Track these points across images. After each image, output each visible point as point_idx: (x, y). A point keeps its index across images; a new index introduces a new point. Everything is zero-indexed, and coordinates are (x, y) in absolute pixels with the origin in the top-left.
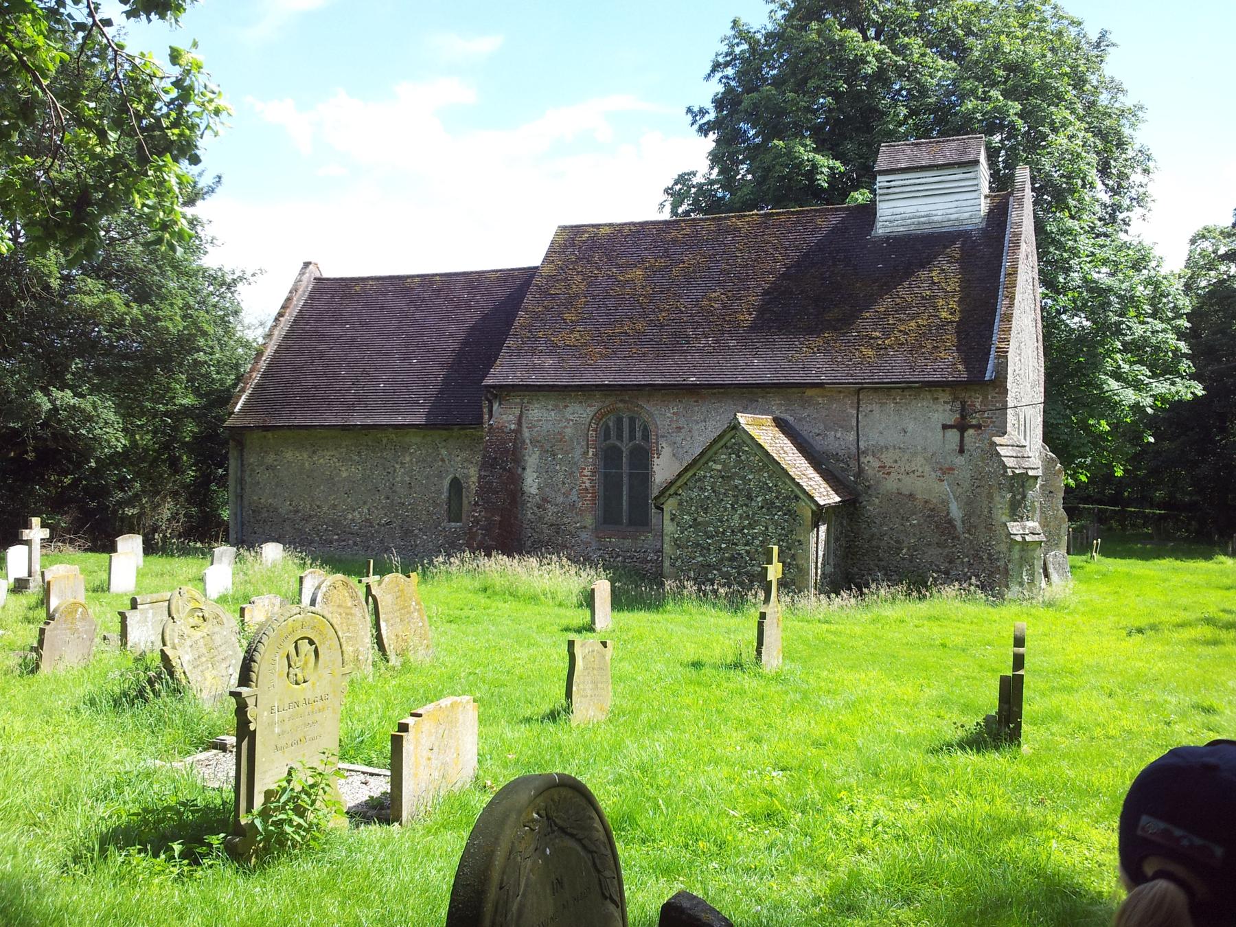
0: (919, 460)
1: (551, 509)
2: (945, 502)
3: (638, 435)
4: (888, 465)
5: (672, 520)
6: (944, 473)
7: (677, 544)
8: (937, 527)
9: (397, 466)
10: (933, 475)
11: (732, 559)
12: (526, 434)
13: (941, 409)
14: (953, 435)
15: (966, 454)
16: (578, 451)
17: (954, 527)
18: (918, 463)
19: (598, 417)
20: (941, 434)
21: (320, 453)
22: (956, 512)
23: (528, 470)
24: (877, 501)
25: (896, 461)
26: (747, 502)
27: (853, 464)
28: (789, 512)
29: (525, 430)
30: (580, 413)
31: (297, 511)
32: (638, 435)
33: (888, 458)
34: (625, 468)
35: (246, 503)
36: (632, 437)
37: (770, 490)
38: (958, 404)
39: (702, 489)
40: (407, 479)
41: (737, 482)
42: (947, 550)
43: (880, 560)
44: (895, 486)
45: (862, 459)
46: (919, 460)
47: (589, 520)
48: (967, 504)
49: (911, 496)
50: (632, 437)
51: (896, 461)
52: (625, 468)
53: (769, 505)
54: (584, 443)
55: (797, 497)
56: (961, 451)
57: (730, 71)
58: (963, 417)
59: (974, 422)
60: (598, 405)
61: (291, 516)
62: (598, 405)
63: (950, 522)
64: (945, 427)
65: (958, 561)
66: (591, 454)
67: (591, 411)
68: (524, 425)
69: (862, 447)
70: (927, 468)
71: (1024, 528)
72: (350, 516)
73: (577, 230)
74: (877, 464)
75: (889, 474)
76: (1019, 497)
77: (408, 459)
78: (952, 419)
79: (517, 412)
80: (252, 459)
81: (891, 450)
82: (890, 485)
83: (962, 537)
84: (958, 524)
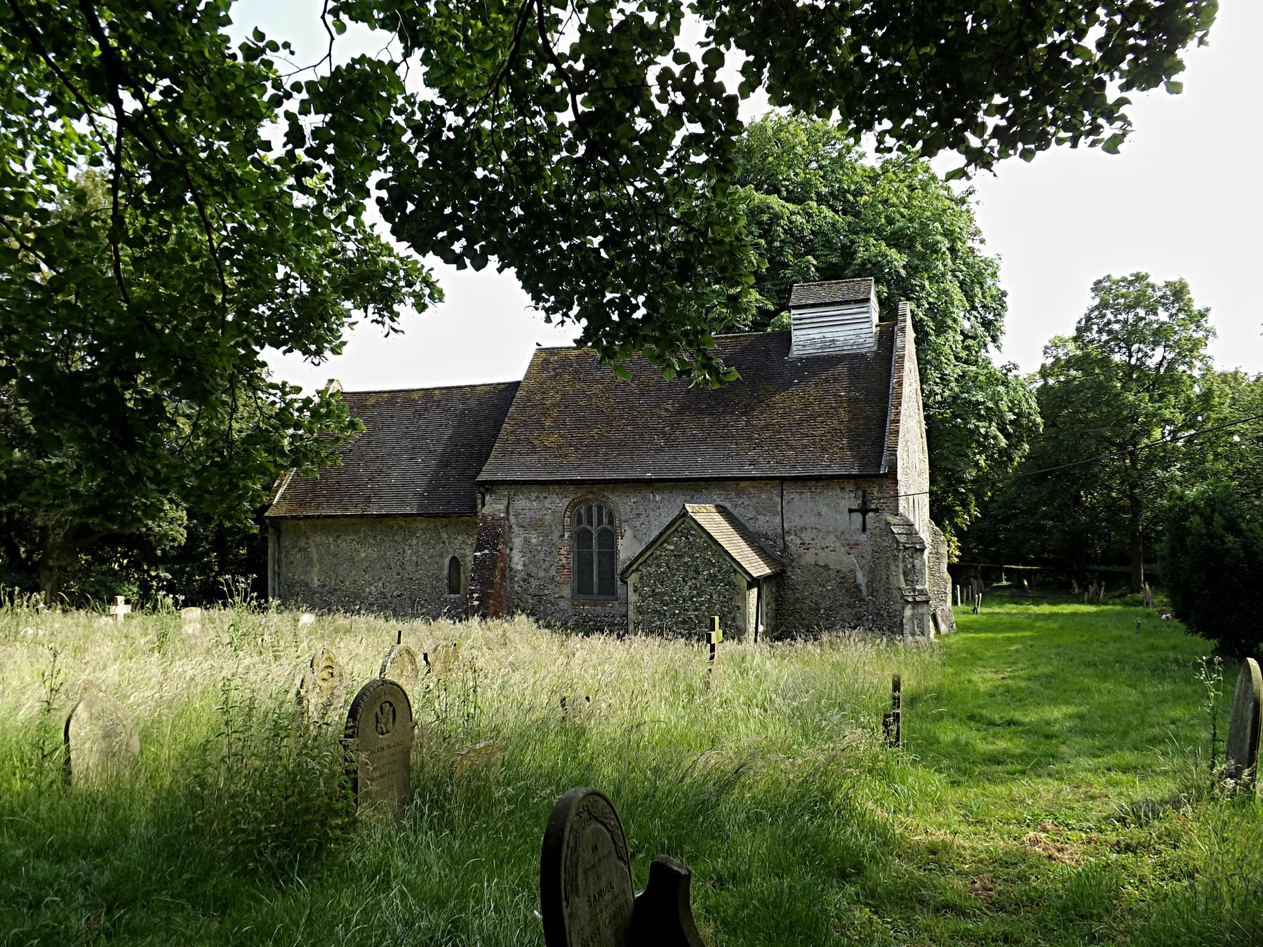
0: (832, 537)
1: (534, 583)
3: (605, 520)
7: (639, 610)
14: (857, 517)
16: (556, 535)
17: (861, 591)
19: (573, 505)
22: (861, 579)
28: (729, 584)
30: (558, 503)
31: (324, 586)
32: (605, 520)
33: (807, 537)
34: (595, 548)
36: (600, 522)
41: (687, 559)
47: (567, 591)
49: (826, 567)
50: (600, 522)
52: (595, 548)
53: (712, 579)
55: (735, 571)
56: (864, 530)
58: (864, 503)
61: (320, 589)
63: (857, 587)
64: (851, 511)
67: (566, 502)
68: (511, 513)
70: (838, 544)
74: (799, 542)
82: (809, 558)
84: (864, 588)
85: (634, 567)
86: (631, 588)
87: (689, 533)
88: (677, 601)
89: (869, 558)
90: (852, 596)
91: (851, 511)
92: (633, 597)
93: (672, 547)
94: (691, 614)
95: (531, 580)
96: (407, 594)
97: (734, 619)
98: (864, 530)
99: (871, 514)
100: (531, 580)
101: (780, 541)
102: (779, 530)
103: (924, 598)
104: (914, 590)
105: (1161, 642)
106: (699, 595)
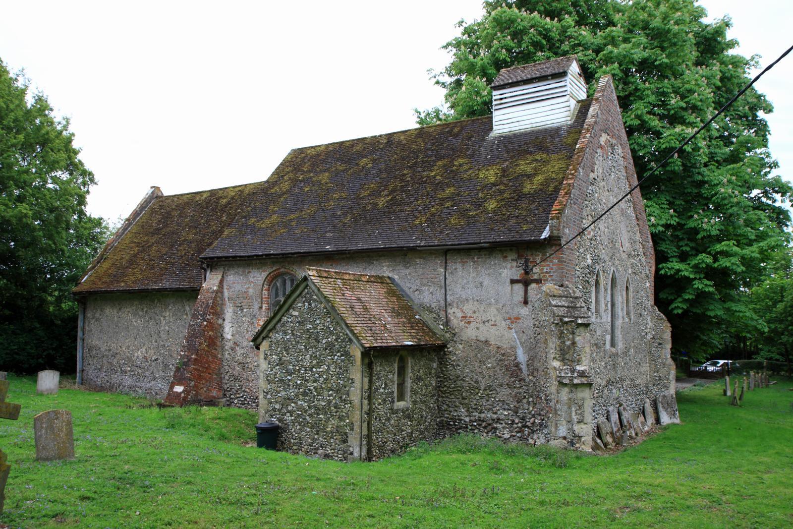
0: (493, 310)
1: (239, 351)
2: (513, 348)
4: (469, 315)
5: (265, 359)
6: (512, 323)
8: (507, 370)
9: (162, 319)
10: (504, 323)
11: (305, 394)
12: (226, 294)
13: (509, 266)
15: (530, 306)
16: (256, 306)
17: (520, 370)
18: (492, 313)
20: (510, 288)
21: (123, 310)
22: (522, 357)
23: (226, 322)
24: (461, 346)
25: (474, 312)
26: (316, 344)
27: (442, 314)
29: (225, 291)
30: (258, 277)
31: (110, 350)
33: (468, 308)
35: (85, 345)
37: (332, 333)
38: (522, 261)
39: (285, 333)
40: (167, 328)
41: (309, 326)
42: (516, 390)
43: (463, 399)
44: (474, 334)
45: (449, 311)
46: (493, 310)
48: (530, 349)
49: (486, 342)
51: (474, 312)
54: (259, 300)
55: (350, 340)
56: (526, 302)
57: (682, 54)
58: (527, 273)
59: (536, 277)
60: (269, 270)
61: (107, 353)
62: (269, 270)
63: (517, 365)
64: (513, 282)
65: (525, 401)
66: (264, 308)
67: (264, 275)
68: (225, 287)
69: (448, 300)
70: (499, 318)
71: (573, 371)
72: (136, 354)
73: (301, 151)
74: (460, 315)
75: (469, 323)
76: (568, 343)
77: (168, 314)
78: (517, 274)
79: (220, 277)
80: (89, 315)
81: (471, 302)
82: (470, 333)
83: (527, 380)
84: (524, 367)
85: (263, 335)
86: (262, 356)
87: (311, 299)
88: (299, 371)
89: (530, 333)
90: (512, 376)
91: (513, 282)
92: (264, 365)
93: (296, 313)
94: (311, 386)
95: (238, 348)
96: (161, 359)
97: (348, 394)
98: (526, 302)
99: (533, 285)
100: (238, 348)
101: (442, 314)
102: (442, 303)
103: (584, 380)
104: (573, 371)
105: (295, 461)
106: (318, 365)
